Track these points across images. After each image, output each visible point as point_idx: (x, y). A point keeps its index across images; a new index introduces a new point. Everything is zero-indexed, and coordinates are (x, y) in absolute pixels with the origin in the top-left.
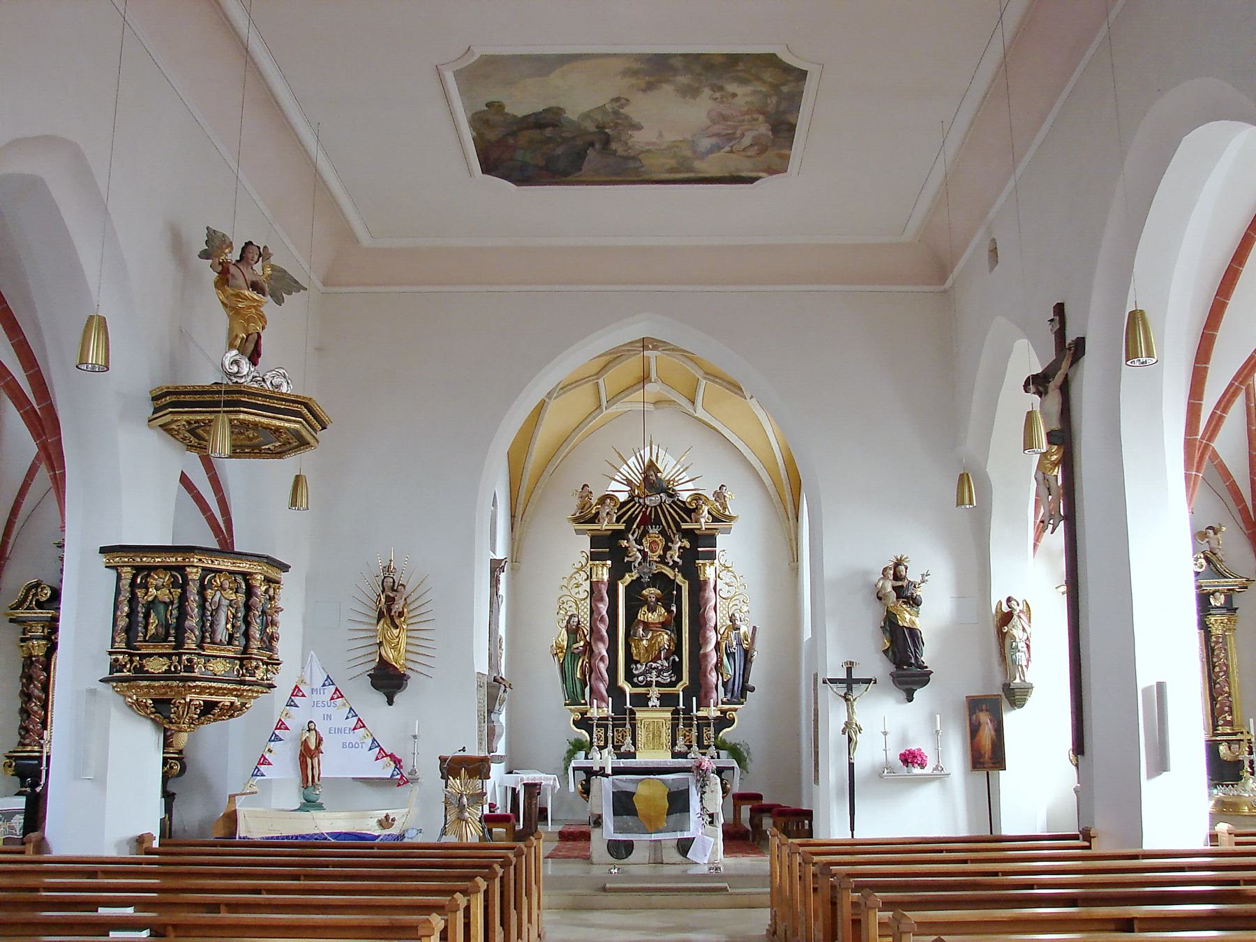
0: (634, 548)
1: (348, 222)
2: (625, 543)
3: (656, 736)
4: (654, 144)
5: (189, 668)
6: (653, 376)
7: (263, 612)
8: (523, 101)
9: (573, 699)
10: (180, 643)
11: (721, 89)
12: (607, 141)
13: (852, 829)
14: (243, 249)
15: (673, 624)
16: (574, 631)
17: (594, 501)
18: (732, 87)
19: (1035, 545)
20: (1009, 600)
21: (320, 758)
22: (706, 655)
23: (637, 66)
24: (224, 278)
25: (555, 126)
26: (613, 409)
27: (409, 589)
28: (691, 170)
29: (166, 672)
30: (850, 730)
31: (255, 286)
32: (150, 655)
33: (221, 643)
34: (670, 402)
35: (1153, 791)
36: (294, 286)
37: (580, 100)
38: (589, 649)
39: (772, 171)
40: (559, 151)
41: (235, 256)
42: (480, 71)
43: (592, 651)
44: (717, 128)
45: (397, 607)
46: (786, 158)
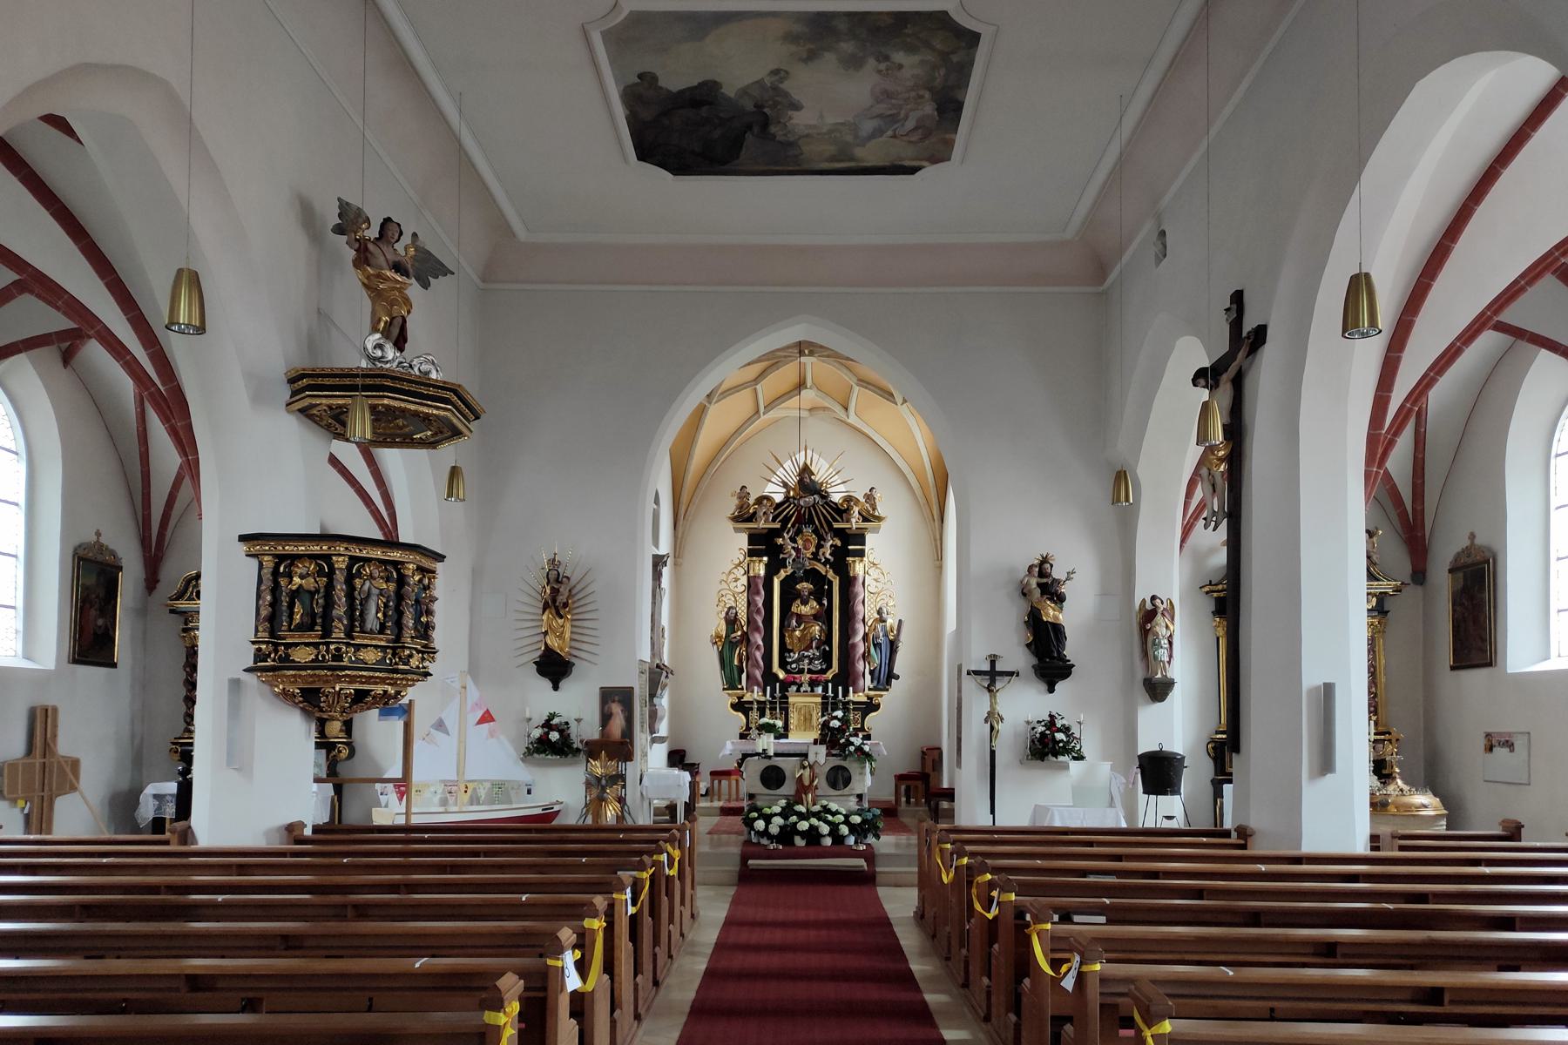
0: (790, 545)
1: (500, 211)
2: (780, 541)
3: (807, 720)
4: (815, 127)
5: (338, 657)
6: (809, 383)
7: (417, 601)
8: (677, 76)
9: (731, 684)
10: (327, 632)
11: (887, 58)
12: (765, 123)
13: (993, 811)
14: (382, 226)
15: (824, 616)
16: (731, 622)
17: (751, 501)
18: (899, 57)
19: (1183, 541)
20: (1153, 598)
21: (455, 756)
22: (854, 646)
23: (797, 28)
24: (363, 257)
25: (710, 104)
26: (773, 414)
27: (573, 581)
28: (852, 159)
29: (316, 660)
30: (992, 718)
31: (398, 267)
32: (297, 645)
33: (372, 632)
34: (825, 409)
35: (1315, 795)
36: (441, 270)
37: (738, 69)
38: (746, 638)
39: (935, 160)
40: (717, 133)
41: (373, 233)
42: (632, 33)
43: (748, 641)
44: (882, 108)
45: (561, 599)
46: (950, 144)
